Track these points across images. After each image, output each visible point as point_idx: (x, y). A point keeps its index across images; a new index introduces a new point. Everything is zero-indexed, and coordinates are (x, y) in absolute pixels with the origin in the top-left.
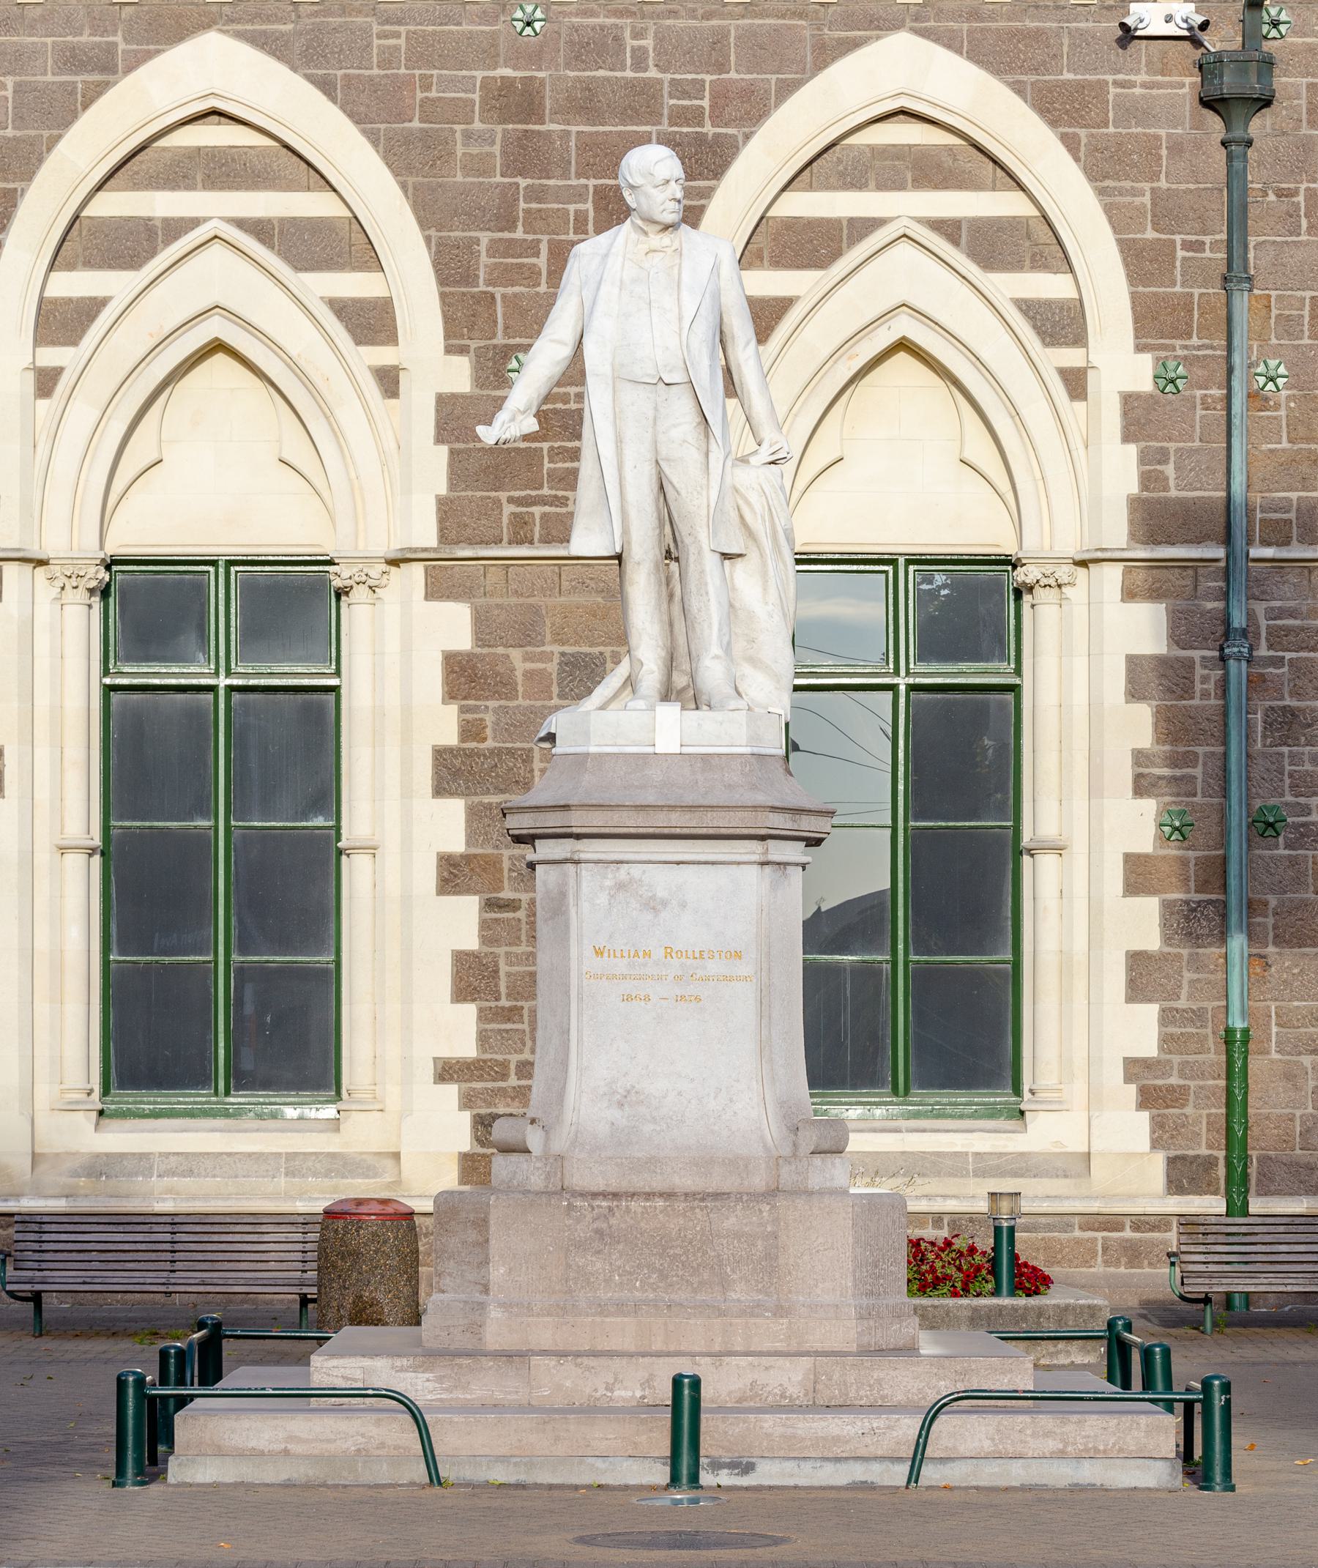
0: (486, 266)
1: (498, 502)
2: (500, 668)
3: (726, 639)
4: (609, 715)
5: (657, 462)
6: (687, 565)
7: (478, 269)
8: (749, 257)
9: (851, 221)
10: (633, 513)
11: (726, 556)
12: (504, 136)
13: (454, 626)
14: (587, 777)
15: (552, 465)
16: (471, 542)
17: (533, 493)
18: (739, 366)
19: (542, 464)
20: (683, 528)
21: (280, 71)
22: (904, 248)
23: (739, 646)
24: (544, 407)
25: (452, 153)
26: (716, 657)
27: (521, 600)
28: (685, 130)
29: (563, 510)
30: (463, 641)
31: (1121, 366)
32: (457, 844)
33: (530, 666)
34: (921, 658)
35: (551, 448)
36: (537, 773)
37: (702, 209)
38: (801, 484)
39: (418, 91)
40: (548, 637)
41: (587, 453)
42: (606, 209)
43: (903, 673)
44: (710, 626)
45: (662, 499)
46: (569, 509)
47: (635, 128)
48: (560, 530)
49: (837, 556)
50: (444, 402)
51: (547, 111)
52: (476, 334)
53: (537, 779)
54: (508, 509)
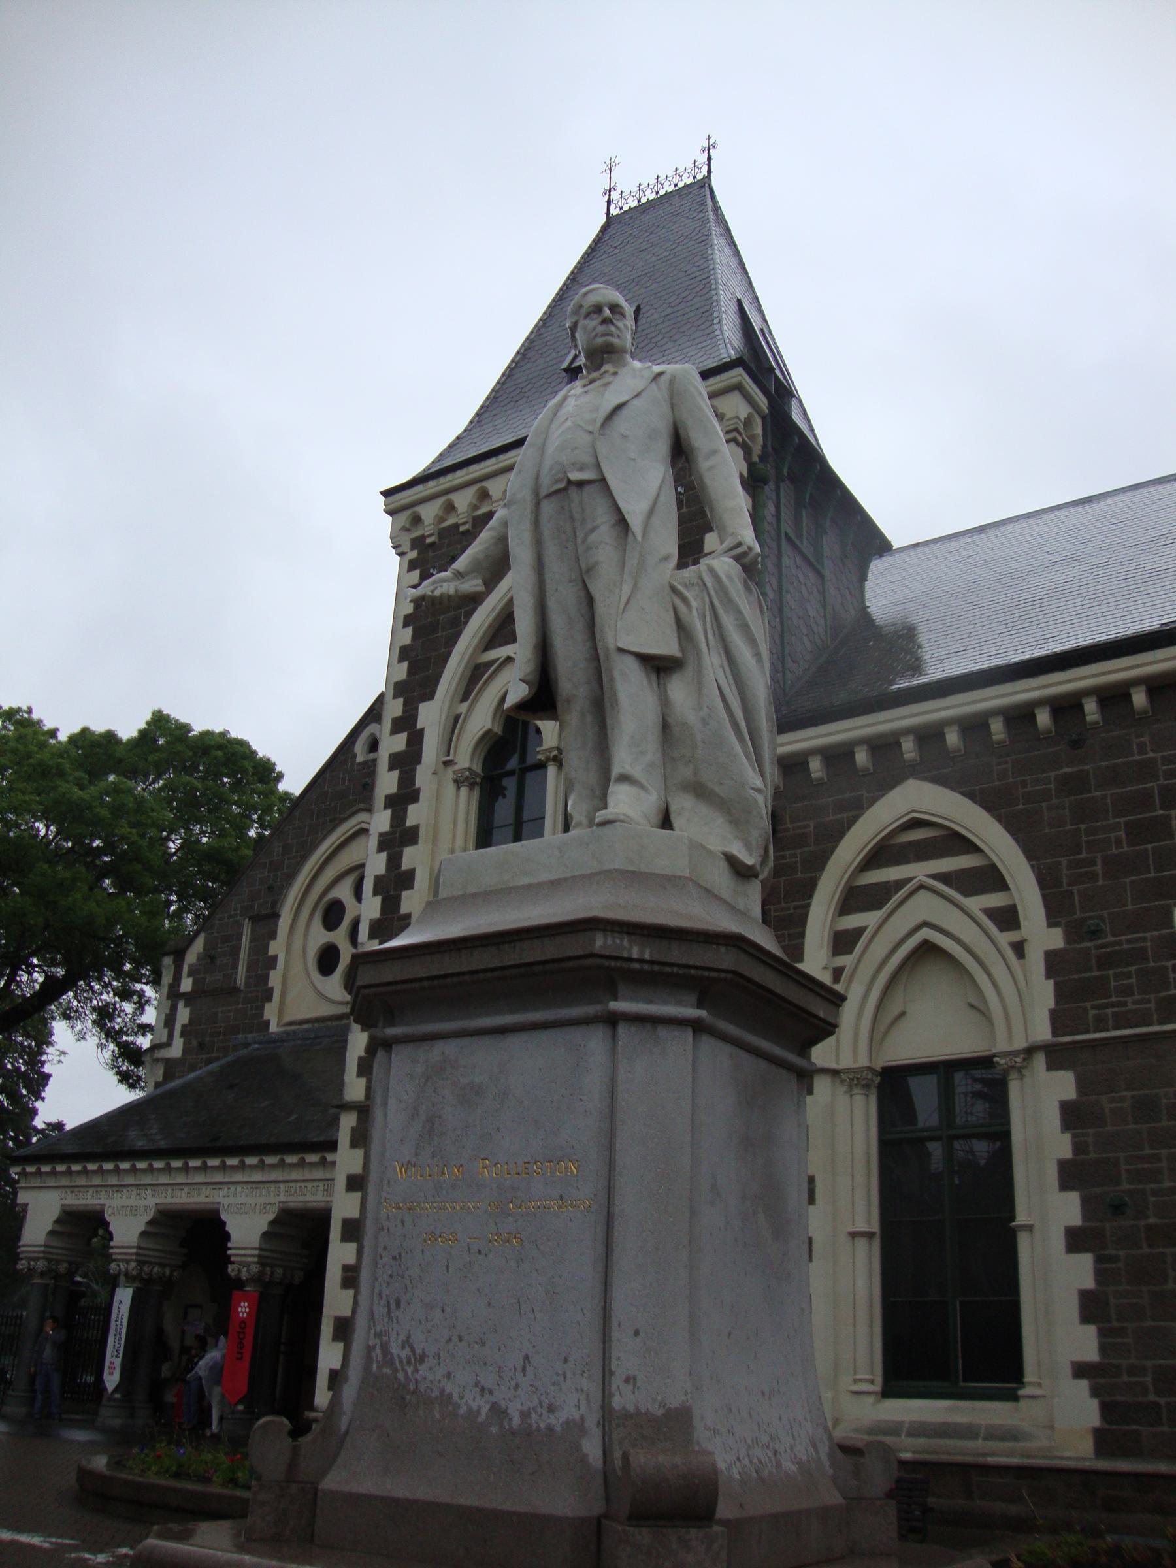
1: (1085, 1010)
21: (947, 793)
30: (1071, 1093)
31: (1042, 935)
32: (1076, 1220)
35: (1115, 974)
54: (1092, 1013)
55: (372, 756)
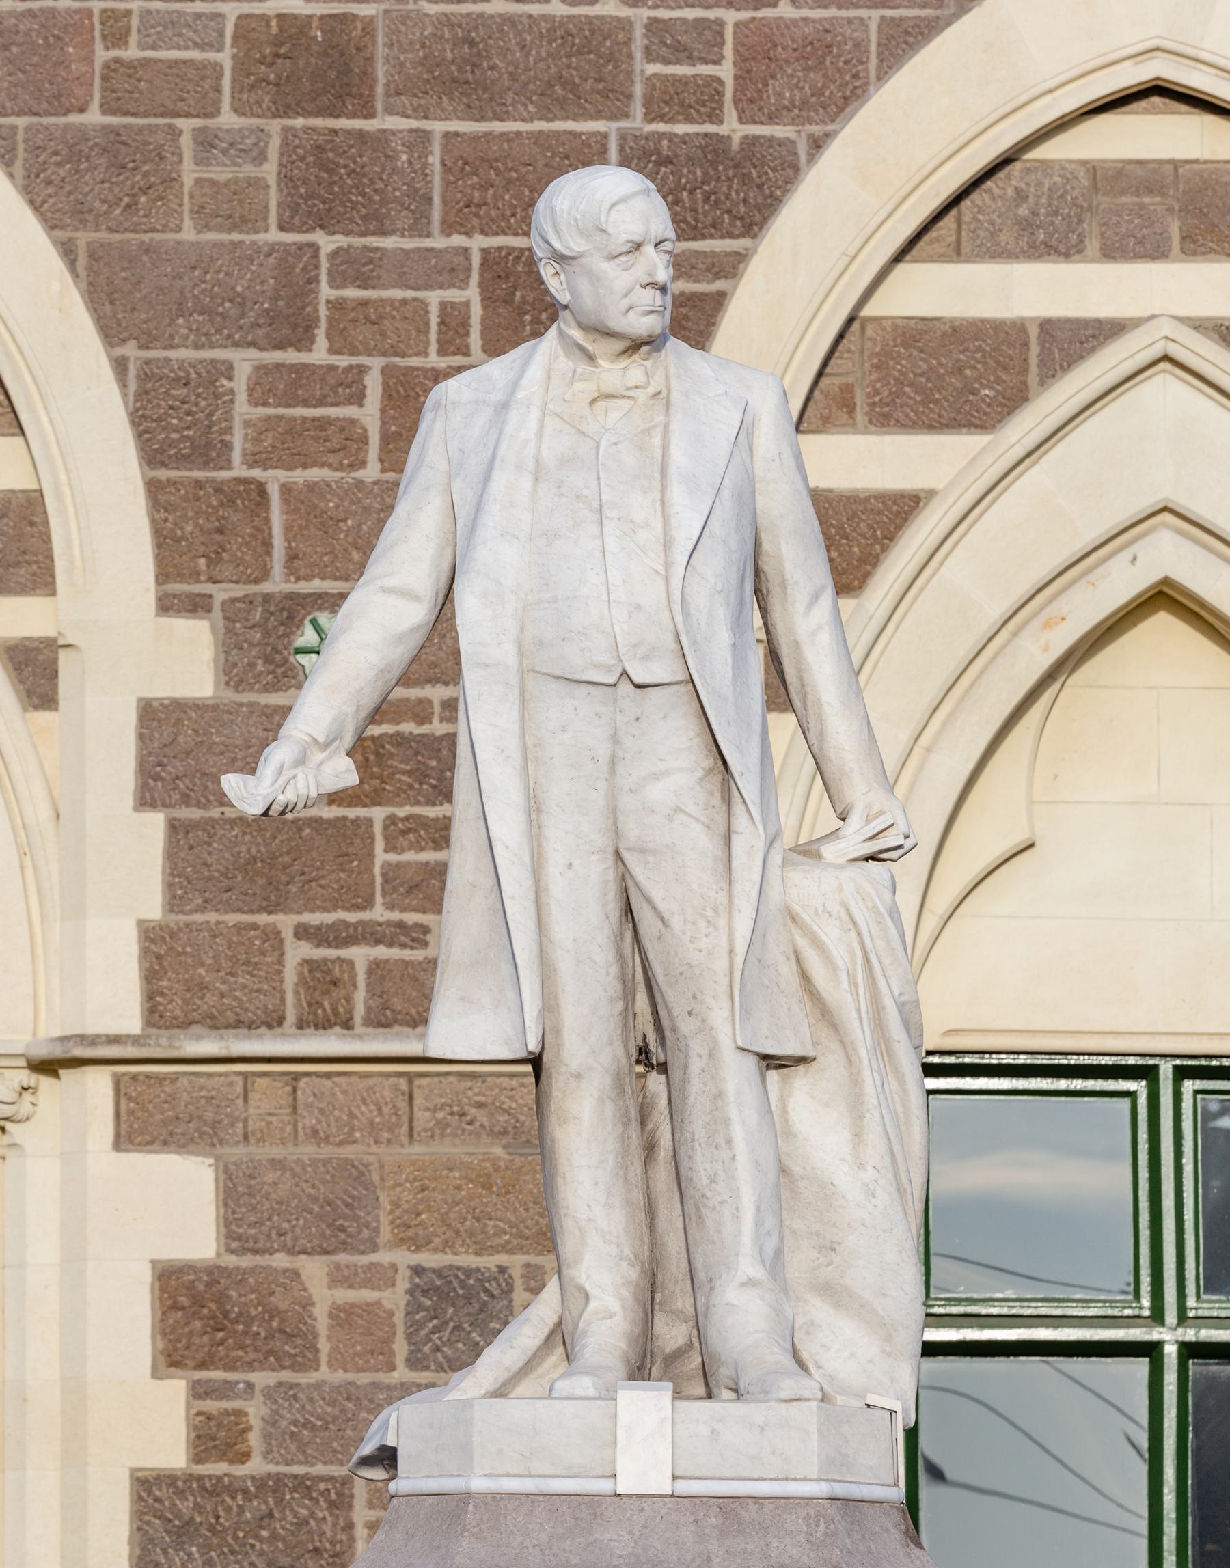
0: (247, 424)
1: (273, 937)
2: (279, 1301)
3: (771, 1244)
4: (515, 1409)
5: (618, 855)
6: (685, 1080)
7: (229, 430)
8: (824, 405)
9: (1048, 326)
10: (565, 964)
11: (770, 1061)
12: (285, 143)
13: (177, 1206)
14: (465, 1544)
15: (392, 857)
16: (215, 1023)
17: (352, 917)
18: (797, 645)
19: (371, 855)
20: (675, 999)
22: (1165, 389)
23: (800, 1260)
24: (375, 730)
25: (171, 181)
26: (750, 1283)
27: (326, 1151)
28: (681, 129)
29: (417, 955)
30: (199, 1240)
33: (345, 1295)
34: (1212, 1284)
35: (391, 821)
36: (360, 1532)
37: (719, 301)
38: (941, 901)
39: (98, 45)
40: (385, 1233)
41: (464, 834)
42: (509, 300)
43: (1171, 1317)
44: (737, 1217)
45: (629, 934)
46: (429, 953)
47: (570, 125)
48: (406, 997)
49: (1022, 1060)
50: (156, 717)
51: (380, 90)
52: (227, 571)
53: (360, 1545)
55: (391, 476)
